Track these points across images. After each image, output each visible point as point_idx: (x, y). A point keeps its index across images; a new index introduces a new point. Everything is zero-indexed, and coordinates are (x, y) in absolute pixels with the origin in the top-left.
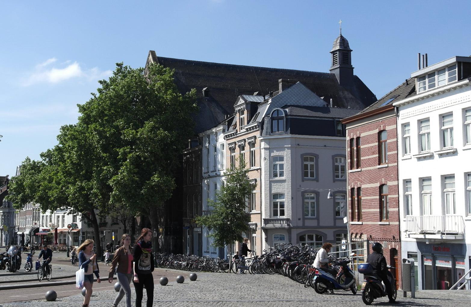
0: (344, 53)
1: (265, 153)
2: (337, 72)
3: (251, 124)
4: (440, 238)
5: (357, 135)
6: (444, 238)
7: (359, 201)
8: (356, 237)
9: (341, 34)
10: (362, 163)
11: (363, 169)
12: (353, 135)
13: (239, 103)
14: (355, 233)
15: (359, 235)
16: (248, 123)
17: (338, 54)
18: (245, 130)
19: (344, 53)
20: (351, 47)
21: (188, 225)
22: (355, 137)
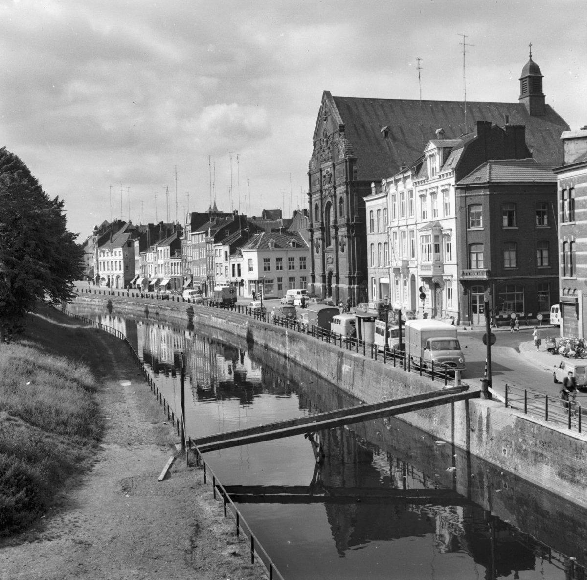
0: (533, 81)
1: (583, 255)
2: (527, 101)
3: (445, 170)
4: (483, 262)
5: (570, 186)
6: (483, 259)
7: (469, 212)
8: (302, 259)
9: (531, 60)
10: (576, 217)
11: (577, 223)
12: (566, 186)
13: (430, 148)
14: (568, 288)
15: (573, 291)
16: (441, 170)
17: (527, 82)
18: (437, 177)
19: (533, 81)
20: (542, 74)
21: (567, 291)
22: (568, 188)
